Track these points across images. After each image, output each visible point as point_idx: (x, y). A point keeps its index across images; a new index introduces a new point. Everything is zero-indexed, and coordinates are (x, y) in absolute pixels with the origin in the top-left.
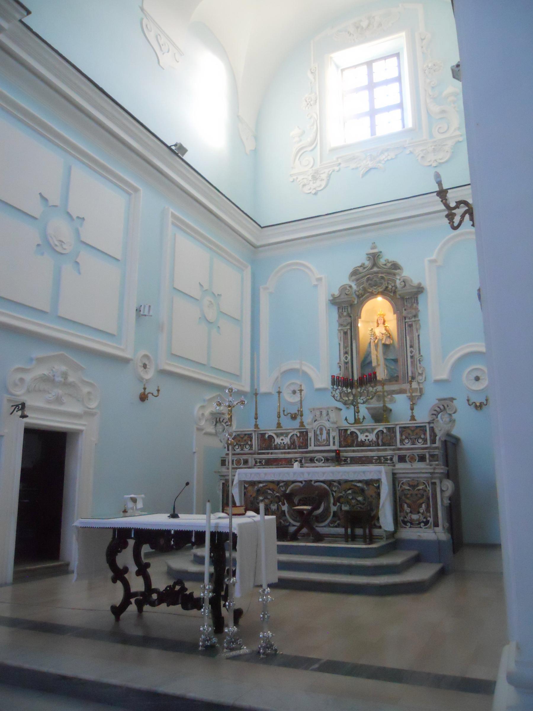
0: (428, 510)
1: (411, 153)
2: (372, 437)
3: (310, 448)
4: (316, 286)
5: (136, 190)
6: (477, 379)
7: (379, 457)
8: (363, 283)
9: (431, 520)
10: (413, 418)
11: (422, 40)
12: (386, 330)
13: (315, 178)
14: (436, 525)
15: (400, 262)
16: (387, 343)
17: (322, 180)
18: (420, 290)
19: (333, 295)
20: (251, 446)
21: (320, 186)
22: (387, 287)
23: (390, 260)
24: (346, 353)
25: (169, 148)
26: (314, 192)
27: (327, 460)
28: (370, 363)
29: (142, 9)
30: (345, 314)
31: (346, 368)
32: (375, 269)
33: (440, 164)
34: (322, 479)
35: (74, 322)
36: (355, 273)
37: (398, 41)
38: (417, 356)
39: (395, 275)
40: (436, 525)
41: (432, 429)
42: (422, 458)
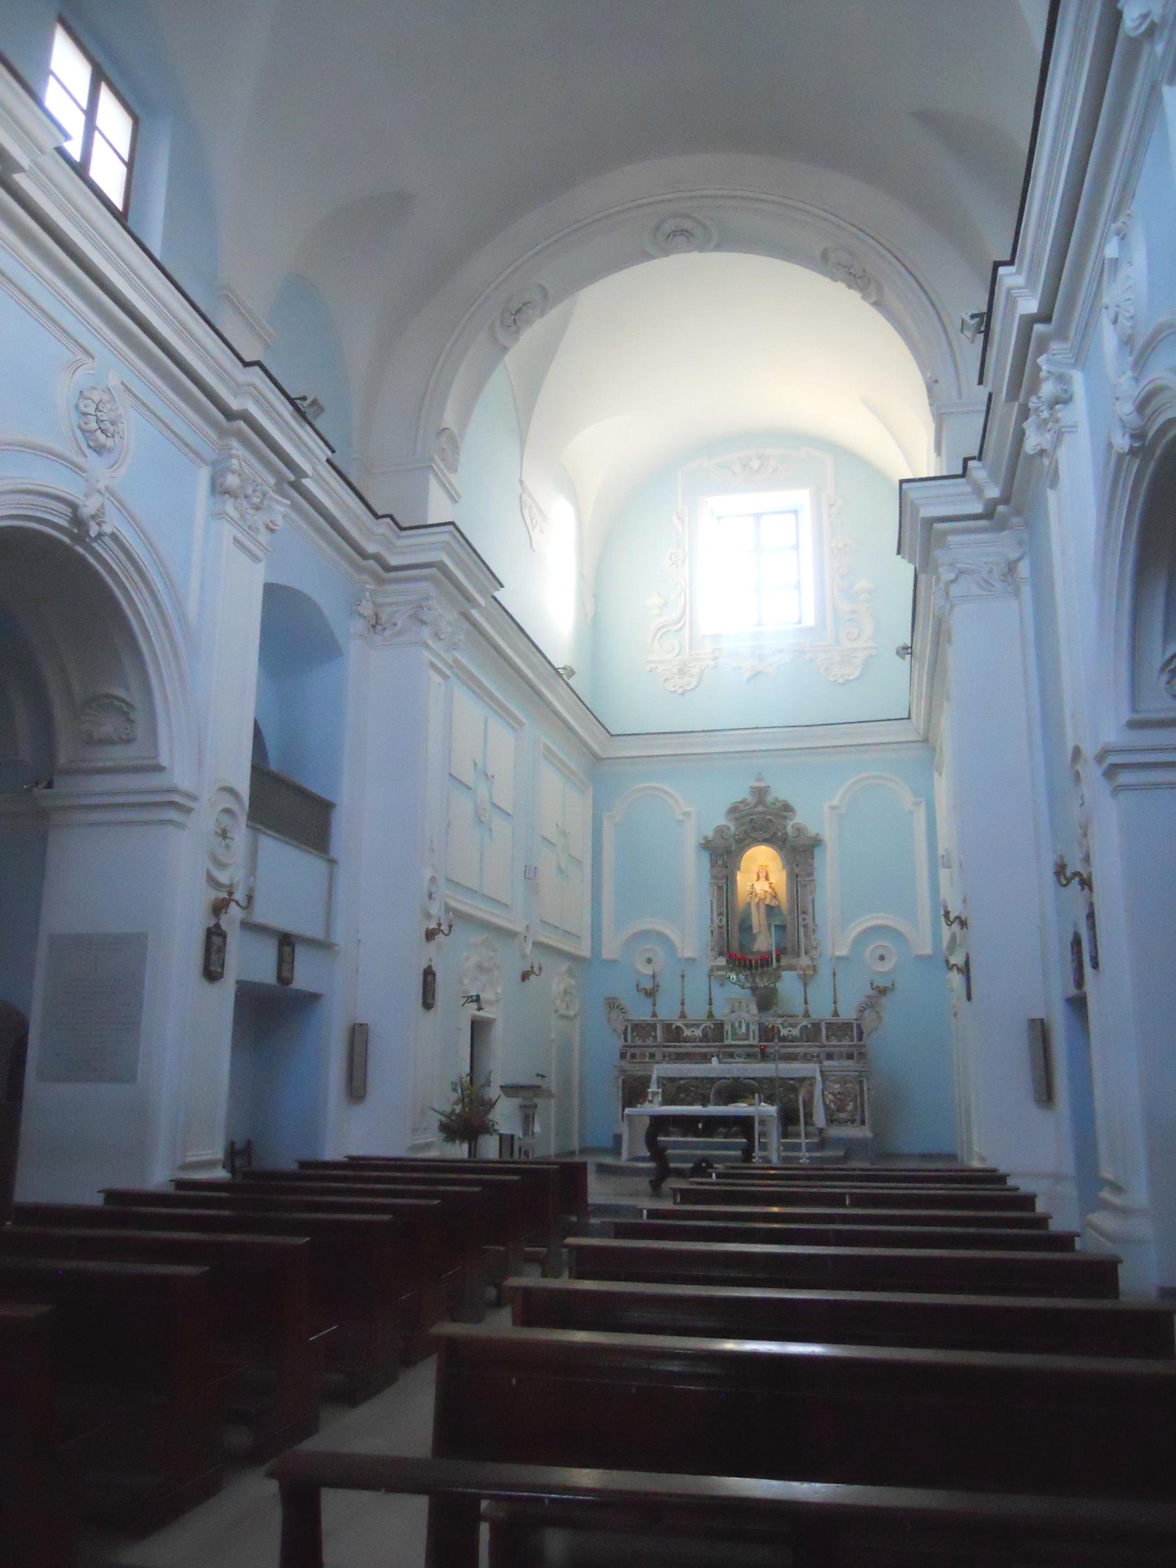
0: (855, 1109)
1: (811, 660)
2: (796, 1032)
3: (727, 1042)
4: (681, 822)
5: (521, 724)
6: (882, 958)
7: (805, 1054)
8: (743, 825)
9: (858, 1118)
10: (836, 1014)
11: (831, 505)
12: (771, 887)
13: (681, 672)
14: (863, 1123)
15: (794, 802)
16: (773, 904)
17: (692, 676)
18: (817, 842)
19: (705, 838)
20: (655, 1037)
21: (689, 684)
22: (775, 834)
23: (781, 798)
24: (720, 914)
25: (556, 670)
26: (680, 691)
27: (748, 1055)
28: (750, 927)
29: (521, 482)
30: (720, 862)
31: (721, 934)
32: (760, 808)
33: (849, 681)
34: (752, 1076)
35: (499, 902)
36: (733, 810)
37: (802, 497)
38: (811, 925)
39: (785, 818)
40: (863, 1123)
41: (859, 1026)
42: (850, 1056)
